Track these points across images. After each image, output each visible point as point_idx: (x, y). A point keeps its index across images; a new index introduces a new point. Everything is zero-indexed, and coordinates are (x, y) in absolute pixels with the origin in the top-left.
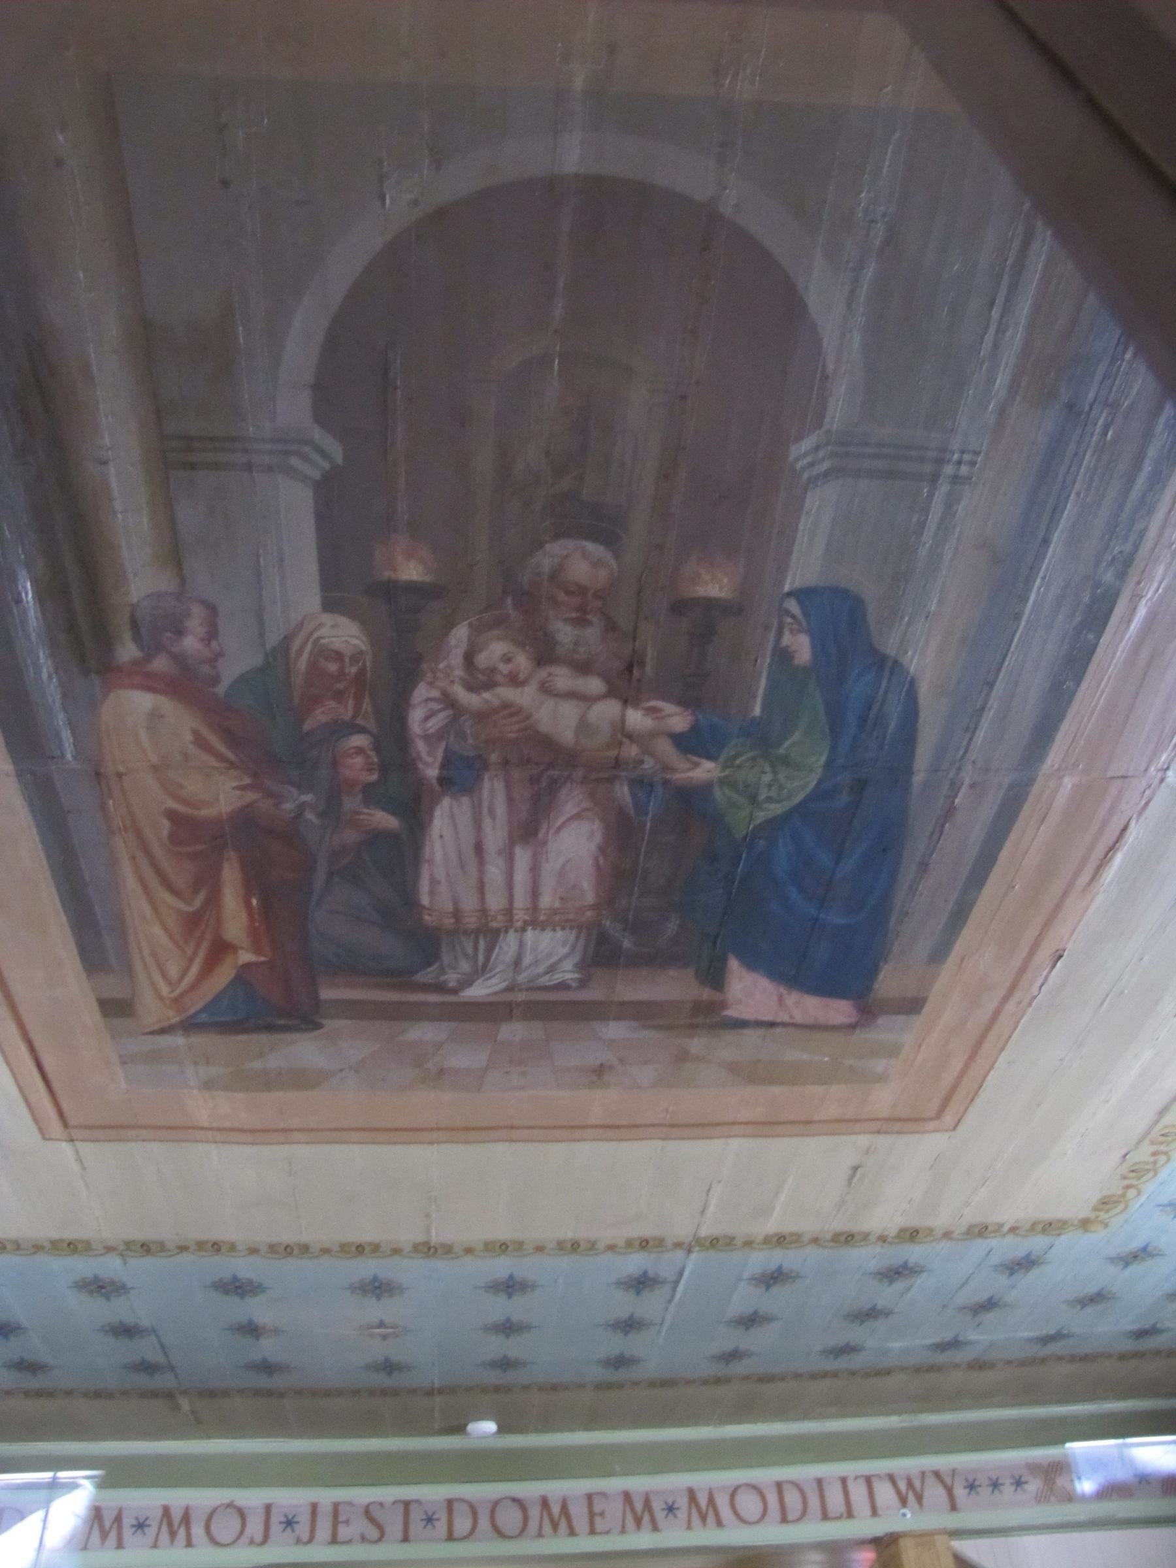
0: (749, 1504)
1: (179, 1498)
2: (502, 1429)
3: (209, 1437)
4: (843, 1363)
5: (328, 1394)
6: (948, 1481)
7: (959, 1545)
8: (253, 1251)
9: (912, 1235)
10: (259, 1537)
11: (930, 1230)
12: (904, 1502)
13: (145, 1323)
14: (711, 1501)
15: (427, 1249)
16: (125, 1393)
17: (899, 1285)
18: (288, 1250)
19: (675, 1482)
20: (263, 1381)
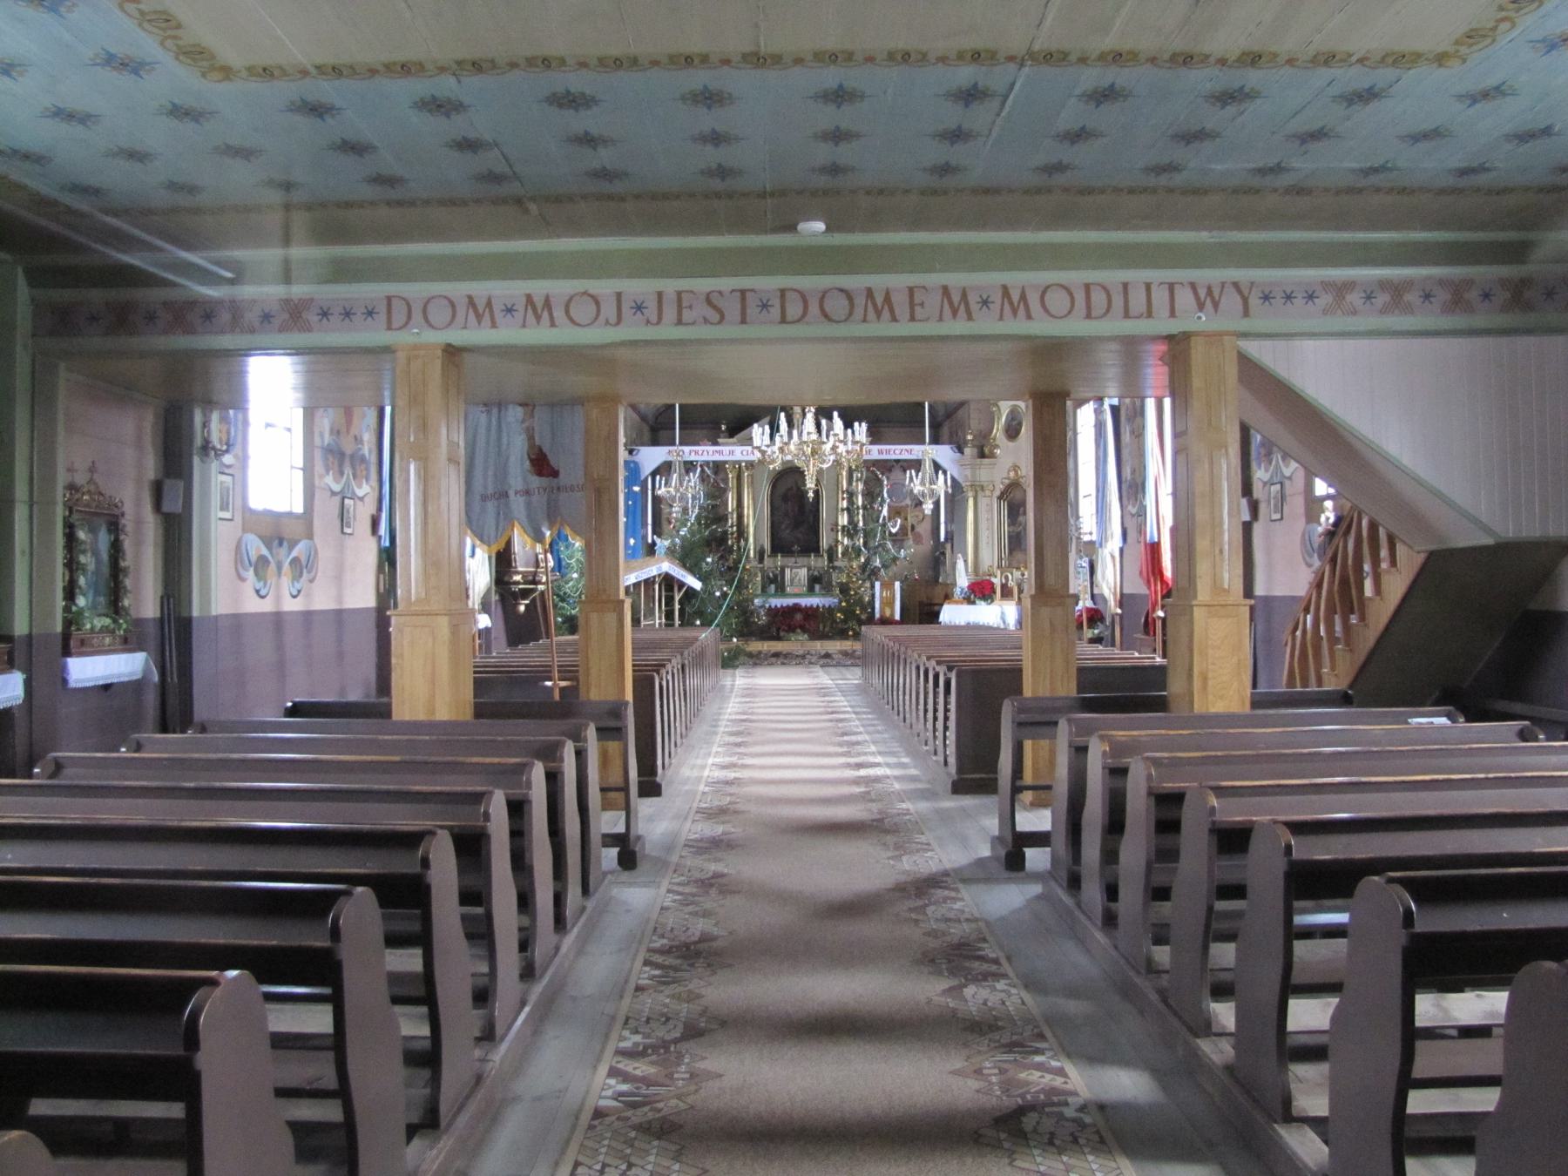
0: (1057, 301)
1: (539, 288)
2: (828, 229)
3: (559, 236)
4: (1163, 180)
5: (666, 196)
6: (1246, 293)
7: (1244, 344)
8: (583, 65)
9: (1253, 59)
10: (613, 320)
11: (1275, 55)
12: (1201, 306)
13: (488, 137)
14: (1023, 297)
15: (756, 59)
16: (478, 201)
17: (1231, 110)
18: (618, 63)
19: (993, 279)
20: (606, 187)
